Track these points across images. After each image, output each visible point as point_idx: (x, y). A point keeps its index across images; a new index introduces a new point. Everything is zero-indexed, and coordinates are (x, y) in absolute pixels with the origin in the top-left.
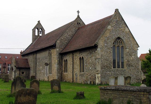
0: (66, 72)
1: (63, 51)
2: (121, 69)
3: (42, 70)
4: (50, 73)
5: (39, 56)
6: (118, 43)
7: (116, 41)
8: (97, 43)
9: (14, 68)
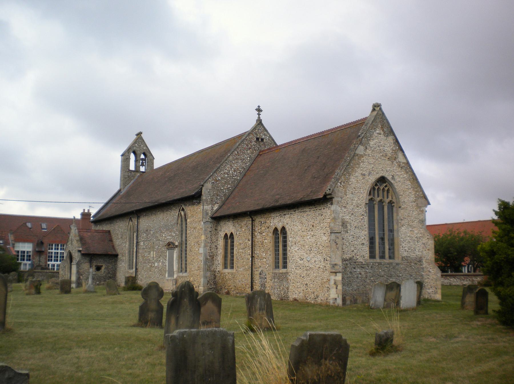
0: (229, 267)
1: (218, 213)
2: (387, 261)
3: (156, 261)
4: (183, 269)
5: (146, 222)
6: (381, 192)
7: (376, 188)
8: (333, 191)
9: (77, 256)
